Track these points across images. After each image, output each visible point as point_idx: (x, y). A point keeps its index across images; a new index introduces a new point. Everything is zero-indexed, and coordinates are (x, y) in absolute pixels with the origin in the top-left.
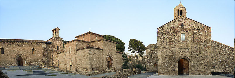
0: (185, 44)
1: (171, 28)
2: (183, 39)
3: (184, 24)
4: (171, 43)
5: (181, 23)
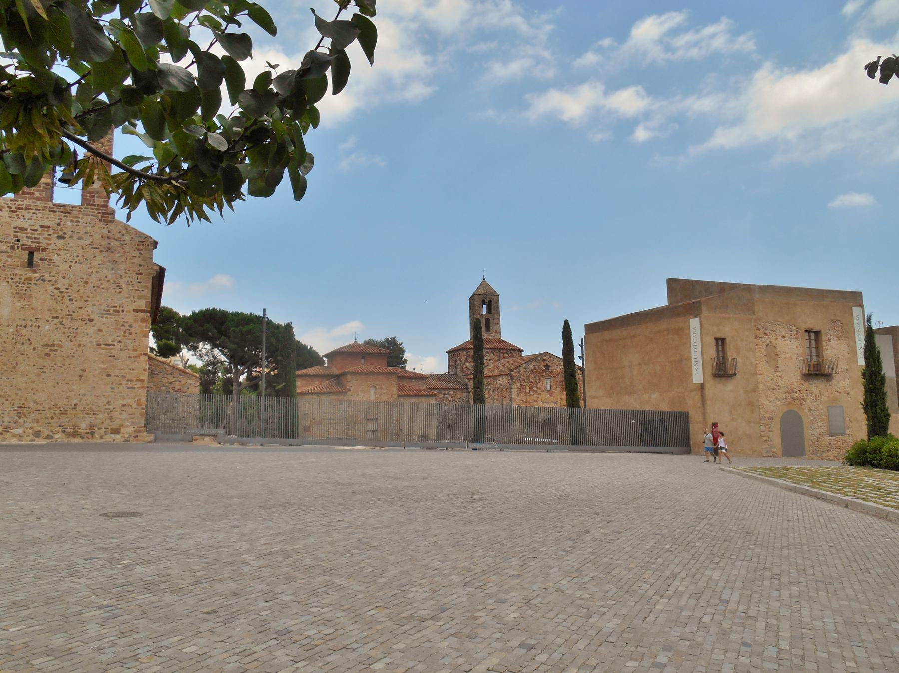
0: (551, 395)
2: (548, 388)
4: (532, 393)
5: (546, 362)
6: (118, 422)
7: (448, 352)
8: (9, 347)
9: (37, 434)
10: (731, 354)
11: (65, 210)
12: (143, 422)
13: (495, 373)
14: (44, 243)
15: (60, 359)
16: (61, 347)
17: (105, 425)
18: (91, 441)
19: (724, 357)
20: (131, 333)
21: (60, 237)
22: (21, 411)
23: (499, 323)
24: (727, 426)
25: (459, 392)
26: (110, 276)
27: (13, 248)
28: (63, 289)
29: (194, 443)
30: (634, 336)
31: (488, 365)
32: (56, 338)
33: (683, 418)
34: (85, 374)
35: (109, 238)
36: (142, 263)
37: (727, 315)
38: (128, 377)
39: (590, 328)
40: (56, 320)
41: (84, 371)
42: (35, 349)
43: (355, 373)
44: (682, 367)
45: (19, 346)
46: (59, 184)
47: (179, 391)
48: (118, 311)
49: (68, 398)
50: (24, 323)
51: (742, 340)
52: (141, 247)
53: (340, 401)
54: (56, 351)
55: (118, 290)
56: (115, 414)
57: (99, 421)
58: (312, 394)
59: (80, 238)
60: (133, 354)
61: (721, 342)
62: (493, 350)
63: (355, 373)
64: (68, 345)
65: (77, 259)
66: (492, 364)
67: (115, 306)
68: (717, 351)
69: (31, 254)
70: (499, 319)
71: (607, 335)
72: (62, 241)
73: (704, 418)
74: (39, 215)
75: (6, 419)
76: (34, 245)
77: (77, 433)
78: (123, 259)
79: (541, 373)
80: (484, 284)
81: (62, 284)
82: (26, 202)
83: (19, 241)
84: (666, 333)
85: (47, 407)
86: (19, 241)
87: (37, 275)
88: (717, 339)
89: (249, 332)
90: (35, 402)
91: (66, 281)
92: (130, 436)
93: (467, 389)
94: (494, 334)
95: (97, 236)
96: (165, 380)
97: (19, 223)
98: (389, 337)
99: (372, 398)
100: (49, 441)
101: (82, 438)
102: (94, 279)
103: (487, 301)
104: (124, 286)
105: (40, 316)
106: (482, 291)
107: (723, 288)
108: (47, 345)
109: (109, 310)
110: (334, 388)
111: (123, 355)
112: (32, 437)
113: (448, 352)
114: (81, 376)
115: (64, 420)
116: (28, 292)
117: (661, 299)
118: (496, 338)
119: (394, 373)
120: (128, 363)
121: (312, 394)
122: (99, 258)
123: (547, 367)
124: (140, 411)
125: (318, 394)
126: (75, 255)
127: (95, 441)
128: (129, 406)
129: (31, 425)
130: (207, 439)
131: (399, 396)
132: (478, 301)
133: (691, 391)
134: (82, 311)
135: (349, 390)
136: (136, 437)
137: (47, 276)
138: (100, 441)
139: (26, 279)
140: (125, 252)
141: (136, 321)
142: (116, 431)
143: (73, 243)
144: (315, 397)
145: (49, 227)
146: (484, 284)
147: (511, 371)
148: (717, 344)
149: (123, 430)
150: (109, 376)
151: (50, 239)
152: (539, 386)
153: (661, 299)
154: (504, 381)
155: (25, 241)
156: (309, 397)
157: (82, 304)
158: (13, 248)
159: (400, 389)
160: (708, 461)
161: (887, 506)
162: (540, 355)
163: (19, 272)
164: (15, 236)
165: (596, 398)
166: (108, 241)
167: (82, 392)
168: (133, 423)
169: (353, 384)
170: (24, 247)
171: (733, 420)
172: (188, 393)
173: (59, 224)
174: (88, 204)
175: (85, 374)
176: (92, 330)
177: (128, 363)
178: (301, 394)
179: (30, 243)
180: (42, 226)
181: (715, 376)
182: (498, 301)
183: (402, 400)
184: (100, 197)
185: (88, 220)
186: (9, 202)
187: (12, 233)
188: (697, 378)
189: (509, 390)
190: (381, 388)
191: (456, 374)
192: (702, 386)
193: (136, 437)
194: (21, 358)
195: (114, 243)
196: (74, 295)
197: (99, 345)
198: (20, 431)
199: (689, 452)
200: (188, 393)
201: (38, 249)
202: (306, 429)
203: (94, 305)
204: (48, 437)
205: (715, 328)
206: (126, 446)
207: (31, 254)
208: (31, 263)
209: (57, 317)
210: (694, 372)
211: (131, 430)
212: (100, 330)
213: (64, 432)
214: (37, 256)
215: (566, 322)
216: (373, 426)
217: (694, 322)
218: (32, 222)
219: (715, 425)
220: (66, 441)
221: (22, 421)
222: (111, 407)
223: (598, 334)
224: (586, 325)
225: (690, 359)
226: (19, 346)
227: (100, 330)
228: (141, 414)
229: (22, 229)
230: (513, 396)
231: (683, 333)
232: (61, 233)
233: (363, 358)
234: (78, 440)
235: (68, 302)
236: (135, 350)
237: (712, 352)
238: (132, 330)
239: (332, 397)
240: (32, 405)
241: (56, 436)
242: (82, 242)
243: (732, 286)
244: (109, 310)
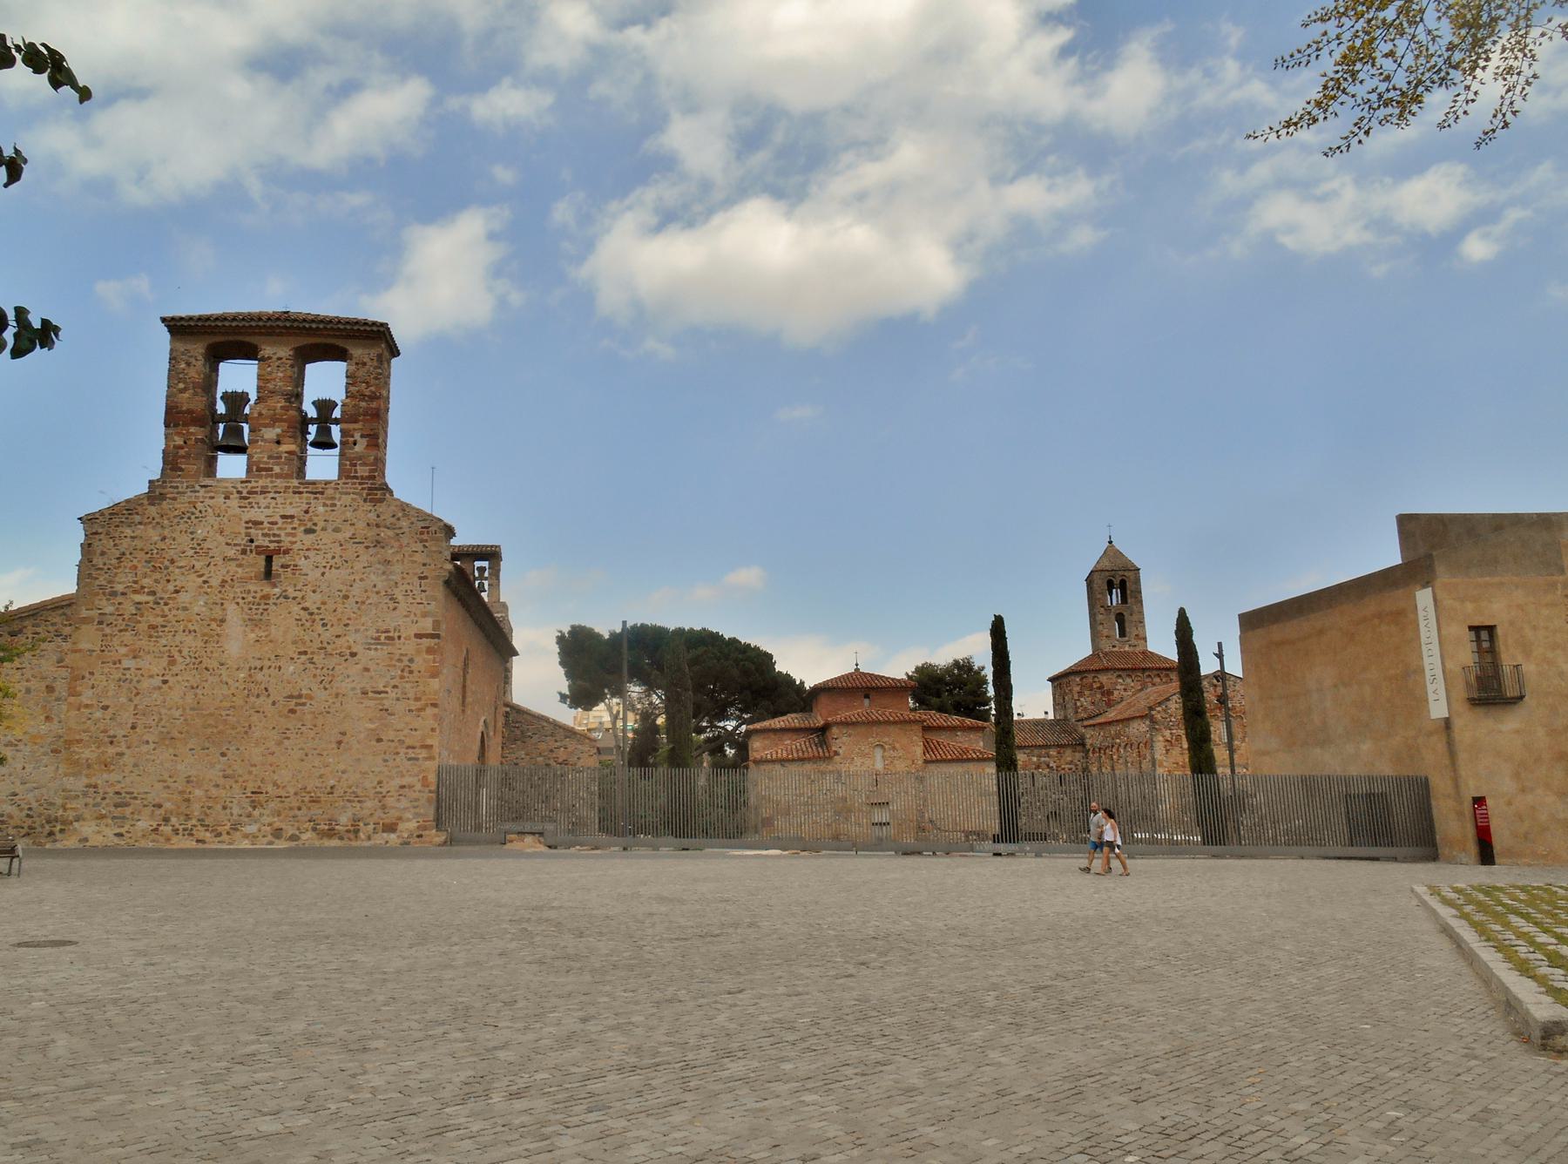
6: (393, 814)
7: (1051, 680)
8: (239, 701)
9: (278, 833)
10: (1509, 657)
11: (318, 489)
12: (431, 813)
13: (1126, 715)
14: (286, 541)
15: (309, 717)
16: (311, 698)
17: (375, 818)
18: (354, 844)
19: (1496, 665)
20: (411, 672)
21: (309, 531)
22: (256, 798)
23: (1142, 622)
24: (1509, 803)
25: (1069, 752)
26: (380, 586)
27: (244, 552)
28: (313, 609)
29: (508, 846)
30: (1321, 632)
32: (306, 684)
33: (1421, 790)
34: (345, 739)
35: (378, 526)
36: (427, 561)
37: (1497, 579)
38: (409, 742)
39: (1252, 622)
40: (303, 657)
41: (344, 734)
42: (274, 703)
43: (846, 724)
44: (1408, 681)
45: (253, 699)
46: (311, 450)
47: (565, 762)
48: (392, 639)
49: (321, 776)
50: (258, 664)
51: (1535, 628)
52: (425, 537)
53: (823, 773)
54: (304, 704)
55: (392, 605)
56: (390, 801)
57: (367, 812)
58: (773, 761)
59: (336, 530)
60: (414, 705)
61: (1484, 634)
63: (846, 724)
64: (321, 695)
65: (332, 562)
67: (387, 631)
68: (1480, 651)
69: (269, 560)
70: (1141, 613)
71: (1277, 632)
72: (311, 536)
73: (1457, 786)
74: (279, 500)
75: (236, 811)
76: (272, 546)
77: (335, 833)
78: (399, 557)
80: (1111, 551)
81: (312, 601)
82: (261, 483)
83: (252, 541)
84: (1376, 621)
85: (292, 791)
86: (252, 541)
87: (277, 590)
88: (1475, 629)
90: (275, 784)
91: (318, 597)
92: (410, 836)
93: (1083, 745)
94: (1133, 642)
95: (361, 525)
96: (543, 746)
97: (254, 514)
99: (879, 766)
100: (293, 844)
101: (341, 838)
102: (356, 591)
103: (1117, 581)
104: (400, 598)
105: (281, 653)
106: (1106, 564)
107: (1500, 523)
108: (291, 697)
109: (378, 638)
110: (812, 751)
111: (400, 707)
112: (270, 838)
113: (1051, 680)
114: (340, 743)
115: (316, 811)
116: (265, 617)
117: (1389, 555)
118: (1137, 650)
119: (915, 722)
120: (407, 719)
121: (773, 761)
122: (364, 558)
124: (426, 795)
125: (782, 761)
126: (329, 556)
127: (358, 843)
128: (411, 787)
129: (269, 820)
130: (529, 839)
131: (926, 762)
132: (1100, 583)
133: (1430, 734)
134: (339, 642)
135: (836, 753)
136: (420, 836)
137: (291, 592)
138: (367, 844)
139: (263, 597)
140: (401, 546)
141: (418, 652)
142: (391, 828)
143: (327, 538)
144: (778, 766)
145: (292, 517)
146: (1111, 551)
147: (1151, 708)
148: (1478, 640)
149: (401, 826)
150: (379, 740)
151: (294, 535)
153: (1389, 555)
154: (1139, 729)
155: (262, 541)
156: (770, 766)
157: (339, 630)
158: (244, 552)
159: (927, 747)
160: (1087, 870)
161: (1524, 969)
163: (252, 588)
164: (248, 535)
165: (1253, 755)
166: (376, 530)
167: (342, 767)
168: (417, 815)
169: (842, 741)
170: (260, 550)
171: (1523, 790)
172: (580, 764)
173: (307, 512)
174: (348, 477)
175: (345, 739)
176: (354, 670)
177: (407, 719)
178: (757, 762)
179: (266, 543)
180: (283, 517)
181: (1475, 702)
182: (1138, 581)
183: (932, 767)
184: (364, 464)
185: (350, 502)
186: (239, 485)
187: (243, 531)
188: (1438, 709)
189: (1150, 744)
190: (894, 748)
191: (1066, 719)
192: (1447, 724)
193: (420, 836)
194: (255, 718)
195: (385, 534)
196: (328, 618)
197: (365, 693)
198: (252, 829)
199: (1434, 857)
200: (580, 764)
201: (278, 552)
202: (767, 822)
203: (357, 631)
204: (293, 838)
205: (1469, 607)
206: (405, 850)
207: (269, 560)
208: (268, 574)
209: (305, 653)
210: (1431, 697)
211: (413, 825)
212: (367, 670)
213: (314, 829)
214: (277, 562)
215: (1182, 612)
216: (881, 816)
217: (1424, 597)
218: (269, 512)
219: (1479, 801)
220: (317, 843)
221: (256, 813)
222: (384, 791)
223: (1260, 632)
224: (1241, 617)
225: (1423, 671)
226: (253, 699)
227: (367, 670)
228: (429, 800)
229: (257, 523)
230: (1157, 756)
231: (1404, 618)
232: (309, 525)
233: (867, 696)
234: (335, 843)
235: (320, 629)
236: (417, 699)
237: (1466, 655)
238: (414, 666)
239: (808, 767)
240: (270, 788)
241: (304, 837)
242: (339, 536)
243: (1517, 520)
244: (378, 638)
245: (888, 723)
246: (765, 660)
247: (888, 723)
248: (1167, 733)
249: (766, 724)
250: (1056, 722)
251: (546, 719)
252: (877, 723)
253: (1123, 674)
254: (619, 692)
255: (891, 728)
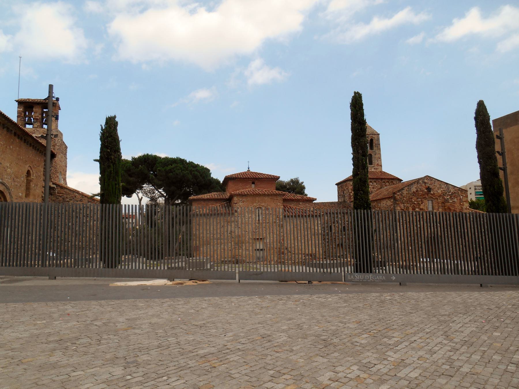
1: (414, 192)
3: (431, 186)
5: (428, 185)
7: (337, 184)
13: (379, 197)
23: (380, 158)
31: (372, 192)
62: (376, 179)
66: (374, 191)
70: (380, 154)
79: (423, 195)
89: (171, 171)
94: (376, 167)
98: (293, 177)
110: (223, 210)
113: (337, 184)
118: (378, 171)
123: (429, 189)
147: (394, 193)
152: (422, 207)
162: (421, 178)
169: (239, 204)
182: (378, 139)
191: (344, 201)
216: (260, 245)
233: (253, 183)
245: (264, 195)
246: (206, 171)
247: (264, 195)
248: (402, 206)
249: (200, 196)
250: (338, 203)
251: (77, 192)
252: (258, 195)
253: (373, 181)
254: (141, 188)
255: (266, 198)
